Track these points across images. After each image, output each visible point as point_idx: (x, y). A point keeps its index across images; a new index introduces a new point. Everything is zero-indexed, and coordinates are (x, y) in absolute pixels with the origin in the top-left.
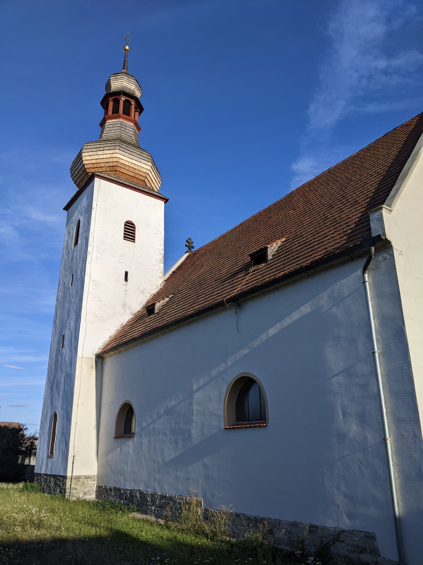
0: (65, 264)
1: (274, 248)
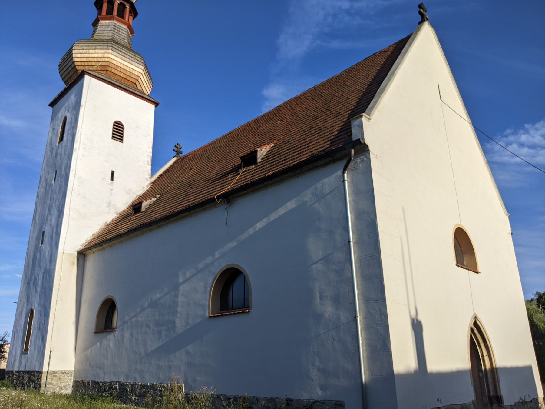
0: (48, 161)
1: (263, 152)
